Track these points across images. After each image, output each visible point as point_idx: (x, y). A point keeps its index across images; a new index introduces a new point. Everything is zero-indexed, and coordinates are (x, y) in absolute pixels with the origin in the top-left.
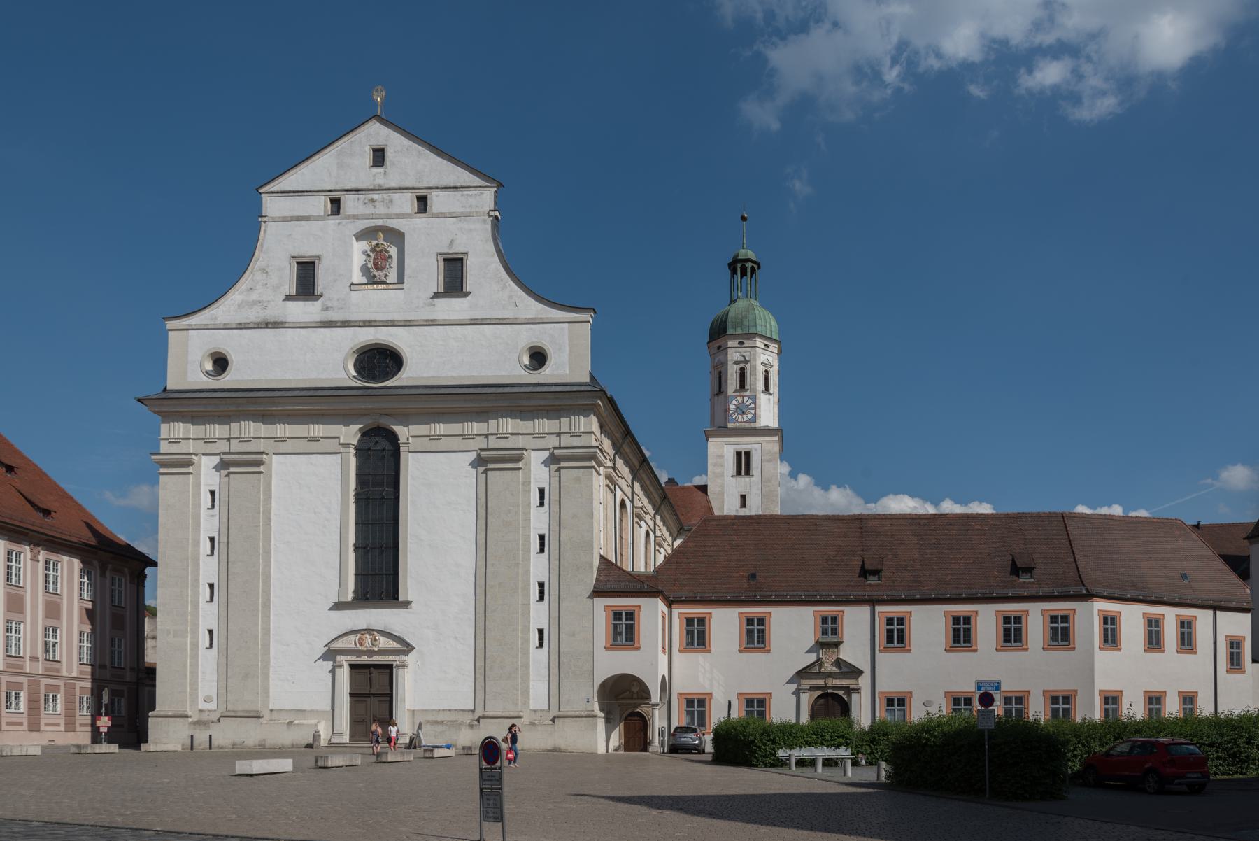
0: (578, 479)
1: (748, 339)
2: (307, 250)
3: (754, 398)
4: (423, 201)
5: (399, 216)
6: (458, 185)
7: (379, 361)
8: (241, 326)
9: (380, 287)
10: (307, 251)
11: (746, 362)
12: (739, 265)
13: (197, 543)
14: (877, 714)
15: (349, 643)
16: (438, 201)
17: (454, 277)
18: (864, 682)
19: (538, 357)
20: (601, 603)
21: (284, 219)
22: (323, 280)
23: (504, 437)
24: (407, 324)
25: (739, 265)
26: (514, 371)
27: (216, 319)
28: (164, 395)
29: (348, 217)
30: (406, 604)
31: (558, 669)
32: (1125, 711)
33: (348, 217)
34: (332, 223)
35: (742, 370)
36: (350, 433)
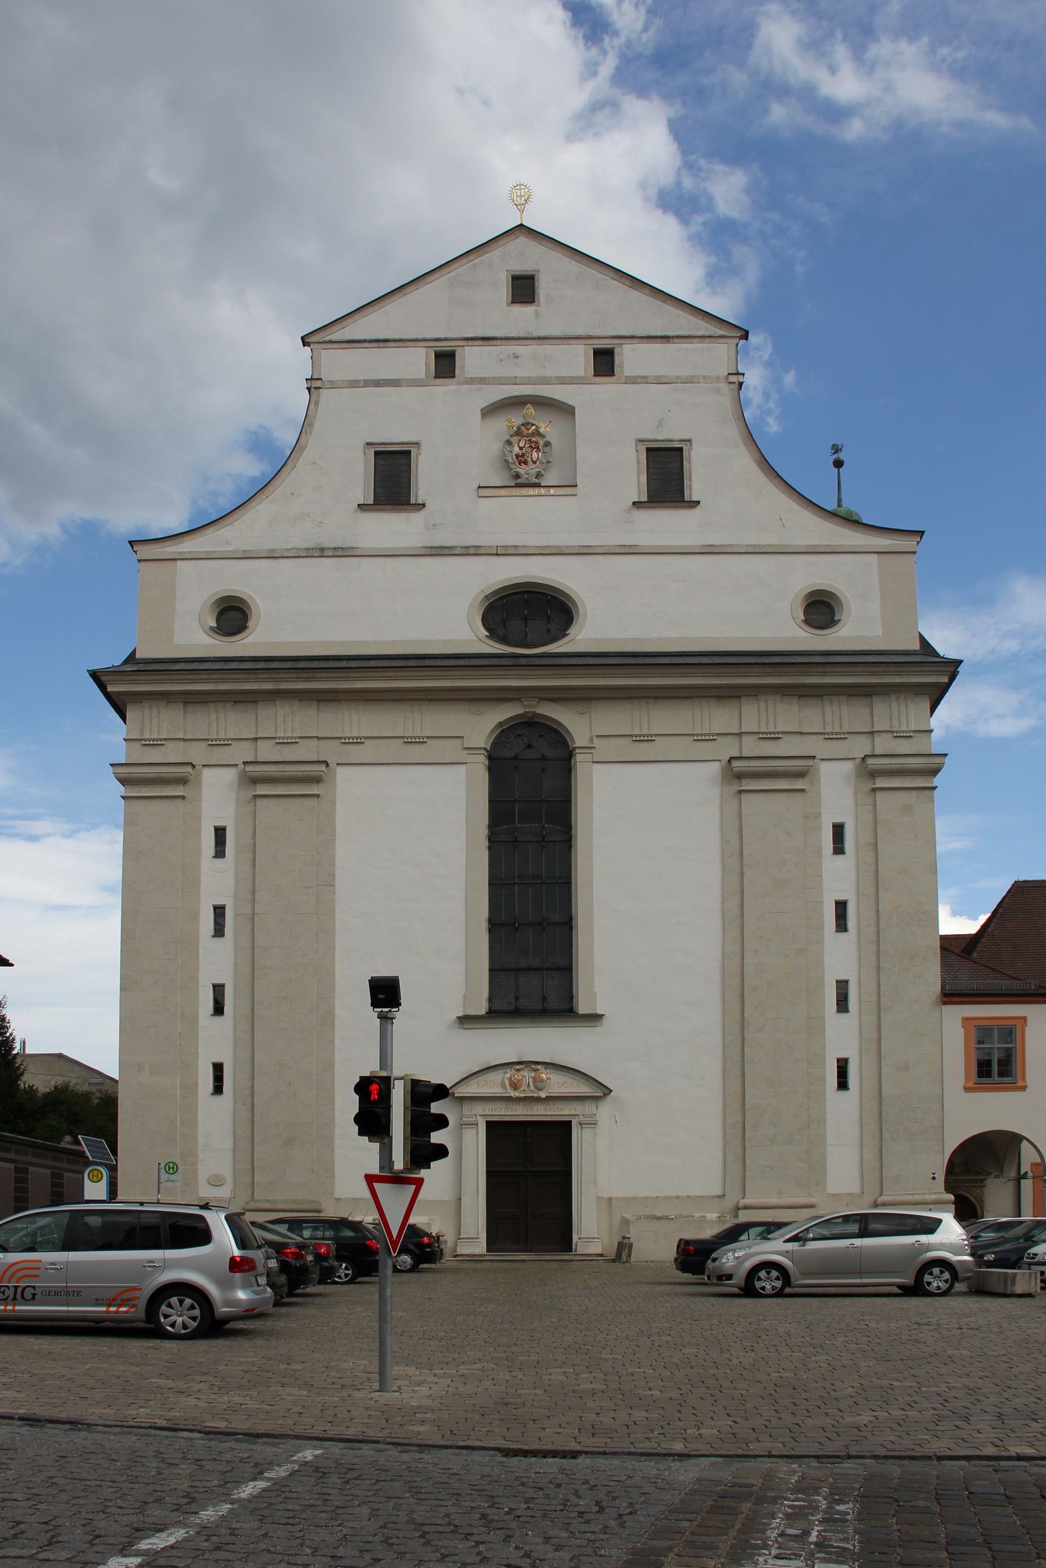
0: (908, 809)
2: (394, 434)
4: (604, 361)
5: (563, 381)
6: (671, 334)
7: (528, 612)
8: (272, 556)
9: (531, 491)
10: (394, 435)
13: (195, 917)
15: (492, 1085)
16: (631, 359)
17: (666, 476)
19: (821, 609)
20: (956, 1014)
21: (353, 384)
22: (425, 481)
23: (773, 737)
24: (584, 552)
26: (788, 632)
27: (228, 543)
28: (128, 668)
29: (471, 381)
30: (595, 1018)
31: (880, 1125)
33: (471, 381)
34: (444, 389)
36: (481, 726)
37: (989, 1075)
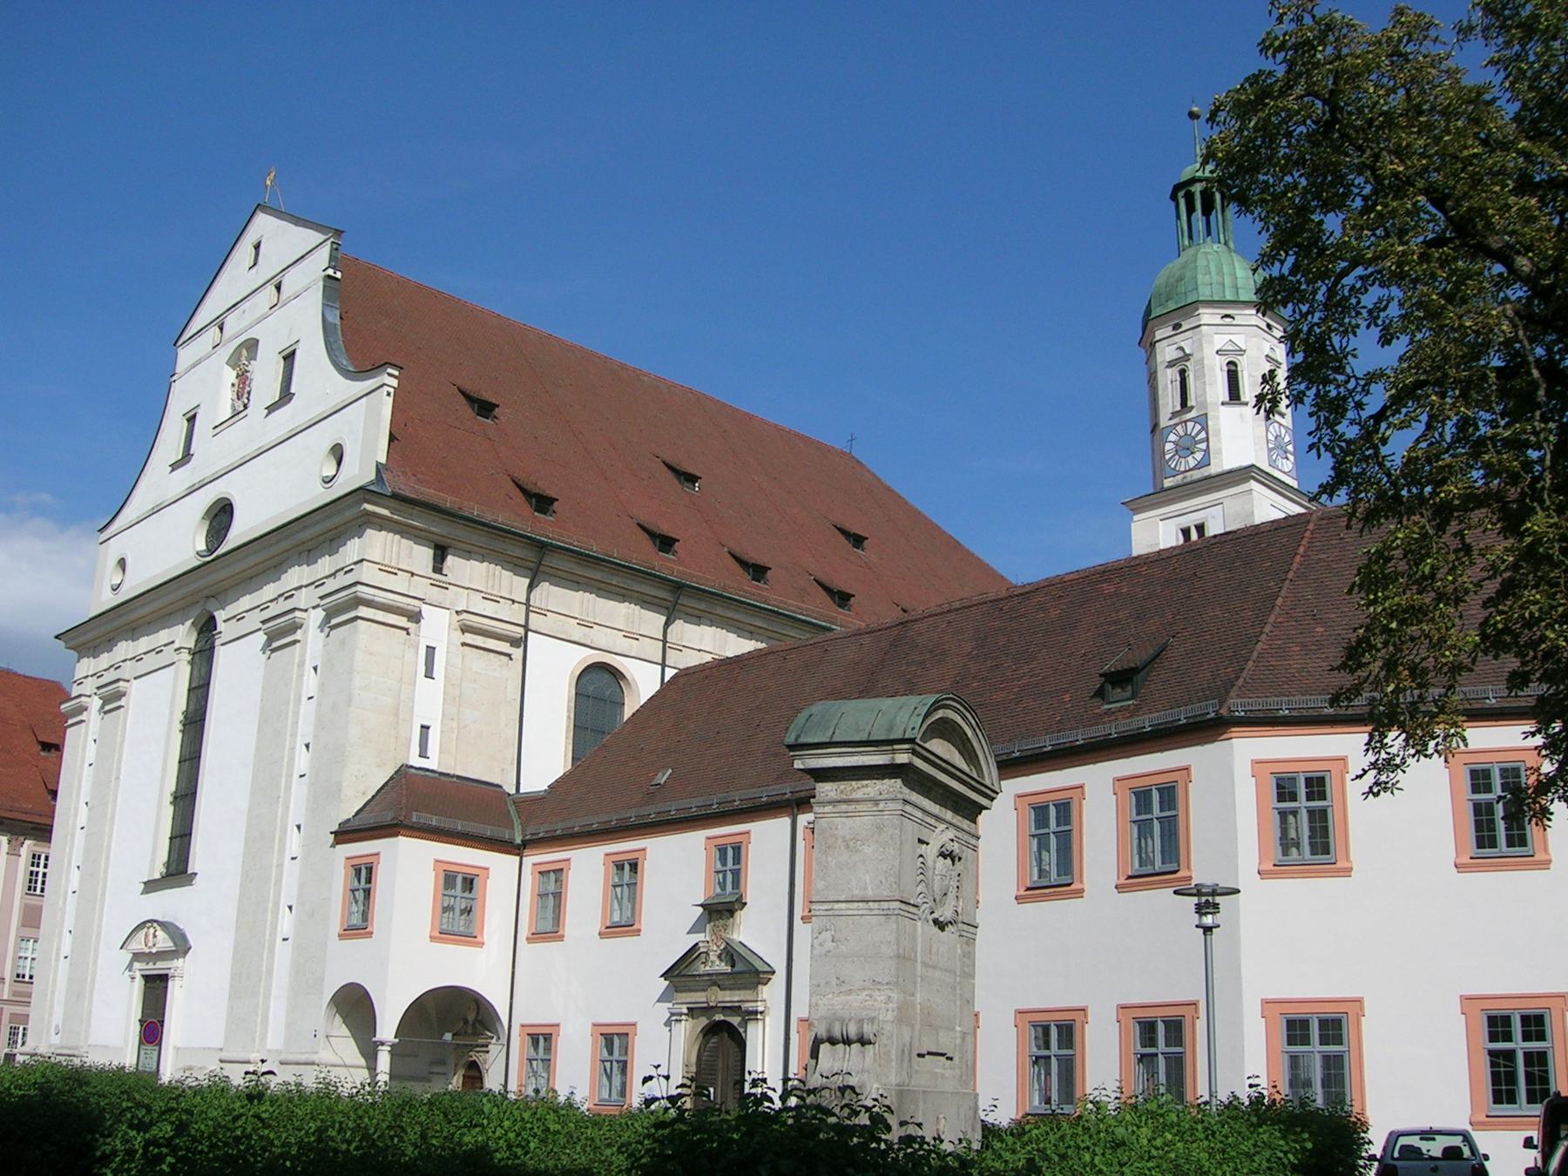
1: (1189, 315)
3: (1203, 420)
11: (1187, 357)
12: (1181, 194)
14: (793, 1069)
18: (771, 995)
25: (1181, 194)
32: (1203, 1091)
35: (1183, 373)
37: (1511, 1098)
